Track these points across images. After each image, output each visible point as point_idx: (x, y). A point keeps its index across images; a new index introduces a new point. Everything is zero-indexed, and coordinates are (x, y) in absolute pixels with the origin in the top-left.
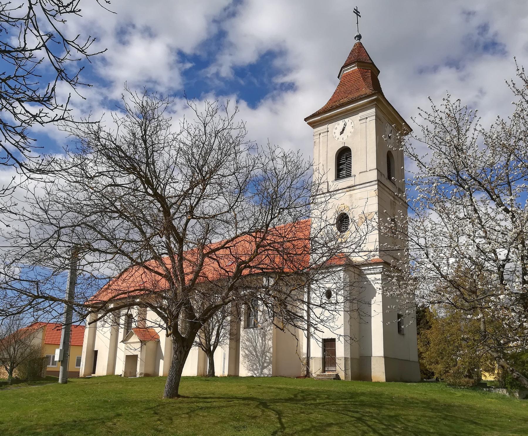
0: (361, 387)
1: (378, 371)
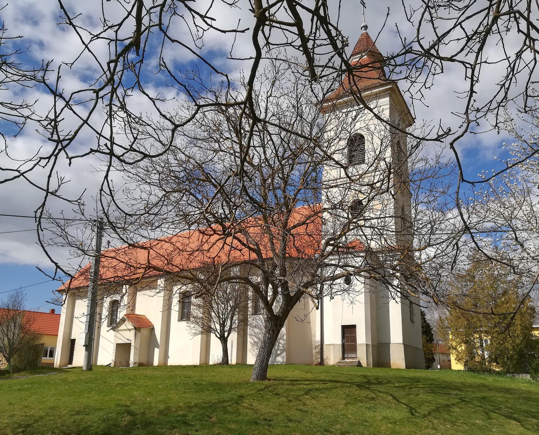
0: (380, 372)
1: (397, 358)
